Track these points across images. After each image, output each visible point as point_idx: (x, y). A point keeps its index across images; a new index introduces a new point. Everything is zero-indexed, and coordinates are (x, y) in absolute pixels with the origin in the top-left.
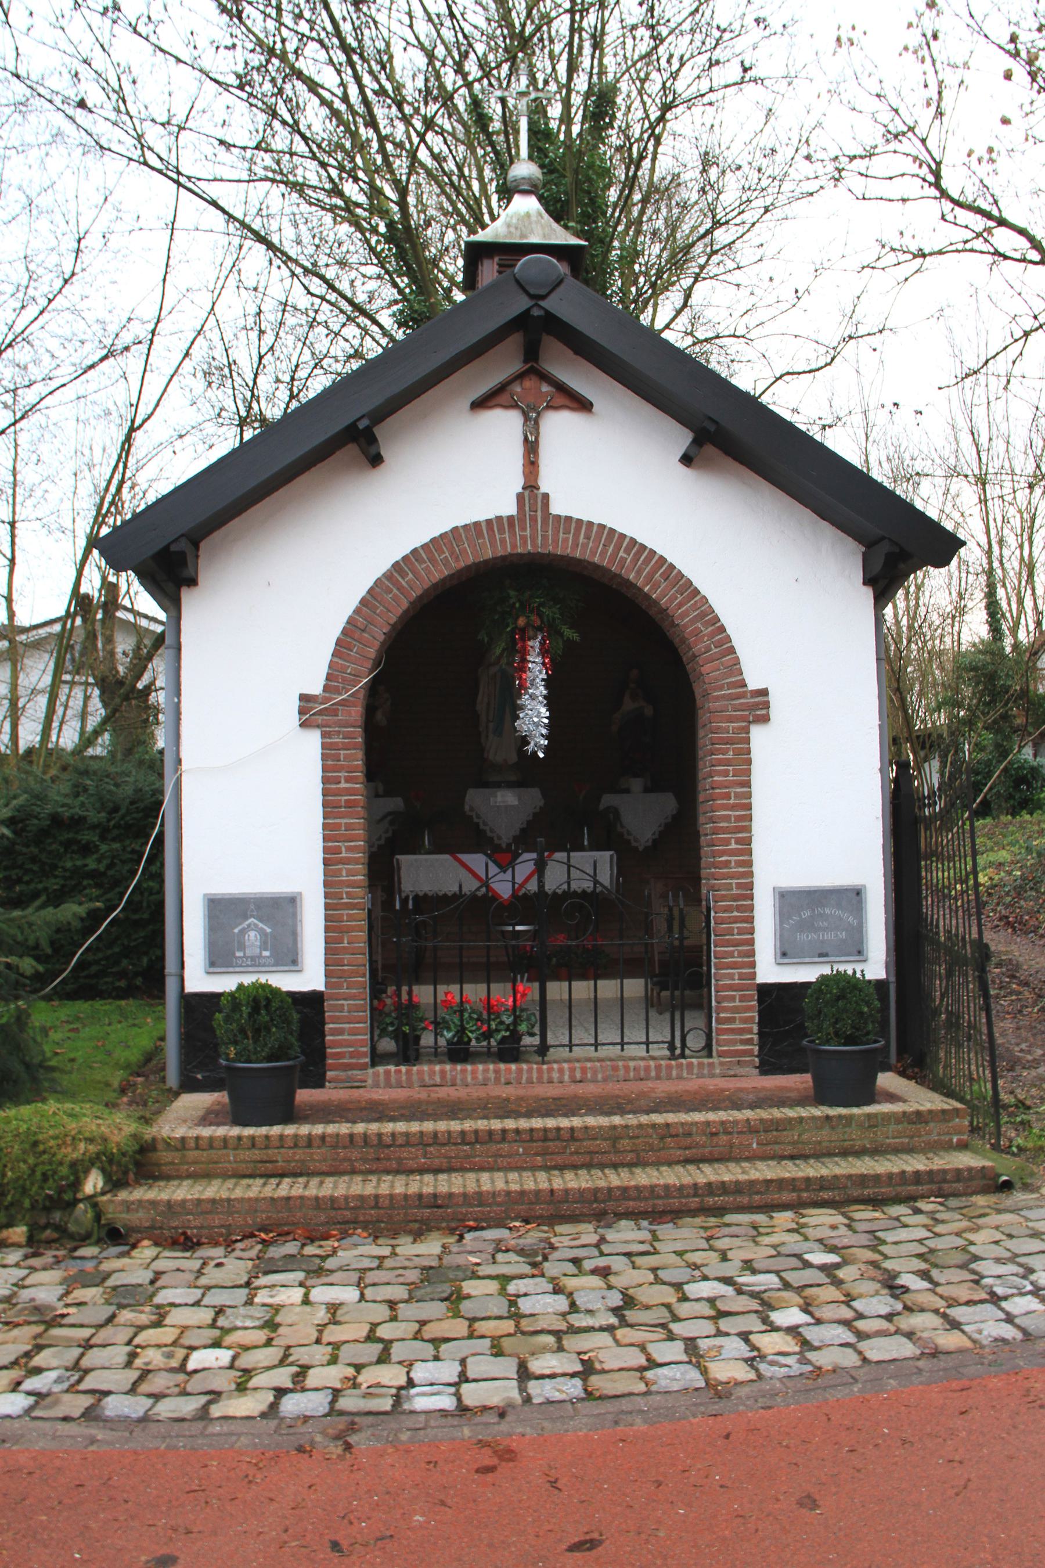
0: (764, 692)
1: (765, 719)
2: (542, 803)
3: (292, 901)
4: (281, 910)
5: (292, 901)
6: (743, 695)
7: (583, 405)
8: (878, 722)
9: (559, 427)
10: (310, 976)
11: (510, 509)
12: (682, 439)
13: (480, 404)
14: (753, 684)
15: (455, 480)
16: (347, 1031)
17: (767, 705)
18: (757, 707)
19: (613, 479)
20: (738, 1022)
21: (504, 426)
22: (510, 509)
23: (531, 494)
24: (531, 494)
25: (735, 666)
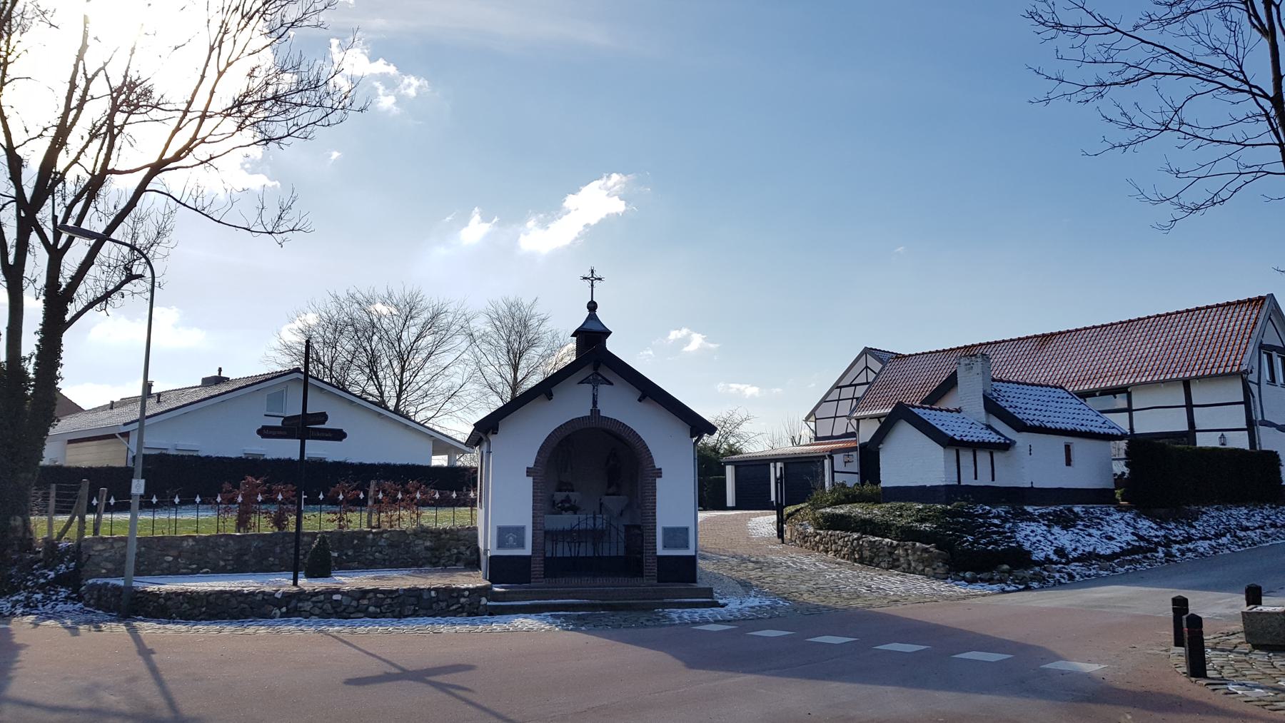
2: (101, 232)
3: (523, 528)
4: (519, 531)
5: (523, 528)
7: (611, 384)
8: (1282, 468)
9: (603, 389)
10: (527, 551)
11: (588, 414)
12: (639, 394)
13: (581, 382)
14: (531, 479)
15: (573, 405)
16: (537, 567)
18: (659, 473)
19: (618, 406)
20: (651, 568)
22: (588, 414)
23: (595, 411)
24: (595, 411)
25: (652, 462)
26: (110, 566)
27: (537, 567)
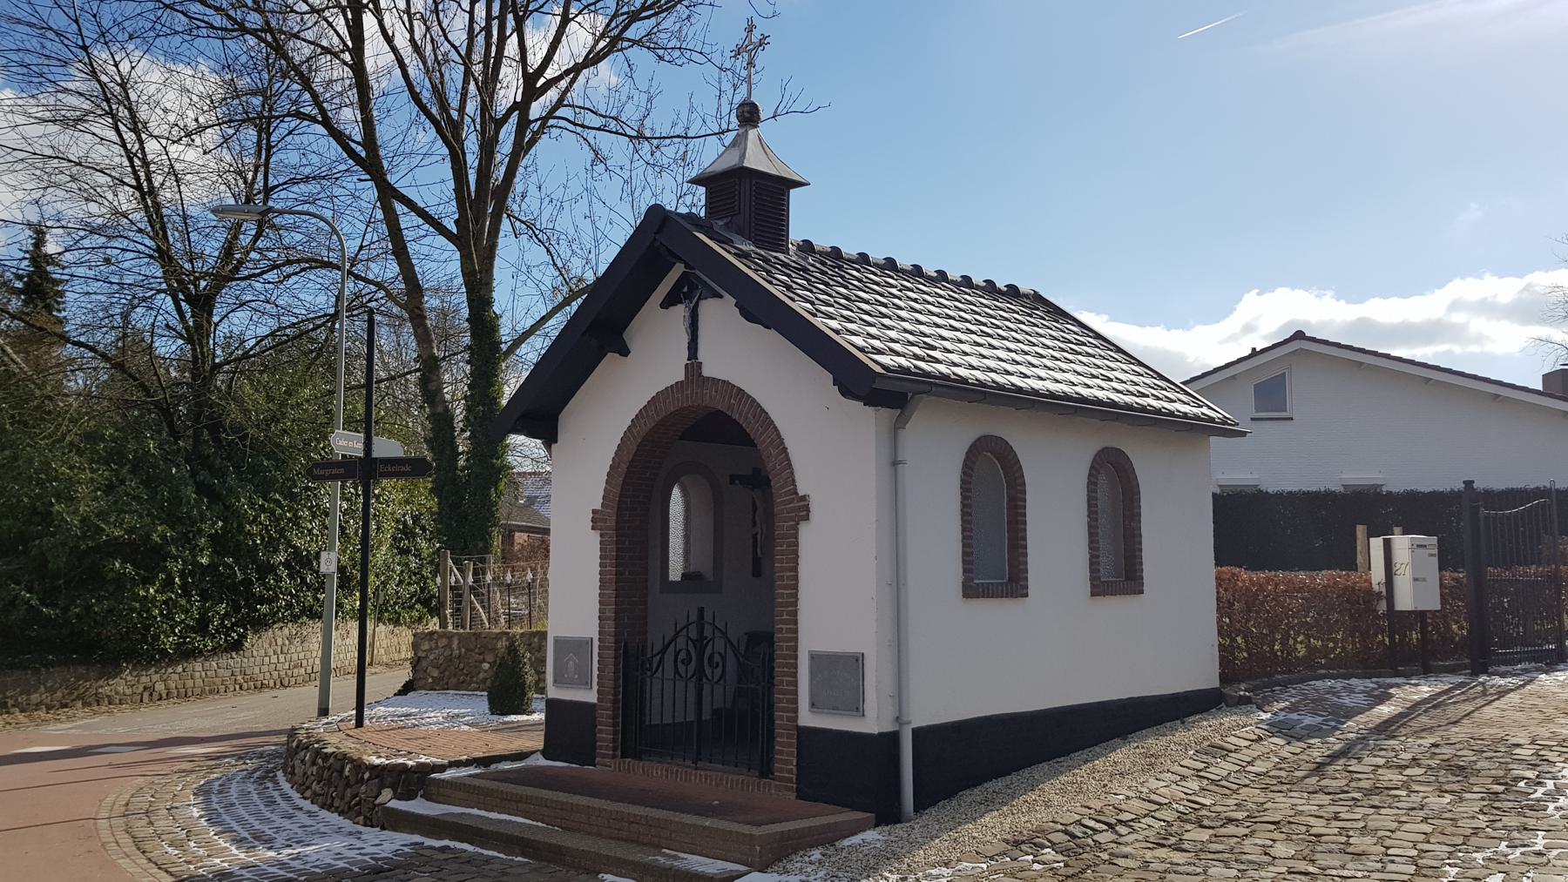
0: (804, 498)
1: (807, 518)
3: (857, 661)
6: (792, 501)
9: (708, 308)
10: (591, 696)
13: (668, 303)
16: (605, 733)
17: (807, 509)
21: (680, 311)
23: (693, 366)
24: (693, 366)
27: (605, 733)
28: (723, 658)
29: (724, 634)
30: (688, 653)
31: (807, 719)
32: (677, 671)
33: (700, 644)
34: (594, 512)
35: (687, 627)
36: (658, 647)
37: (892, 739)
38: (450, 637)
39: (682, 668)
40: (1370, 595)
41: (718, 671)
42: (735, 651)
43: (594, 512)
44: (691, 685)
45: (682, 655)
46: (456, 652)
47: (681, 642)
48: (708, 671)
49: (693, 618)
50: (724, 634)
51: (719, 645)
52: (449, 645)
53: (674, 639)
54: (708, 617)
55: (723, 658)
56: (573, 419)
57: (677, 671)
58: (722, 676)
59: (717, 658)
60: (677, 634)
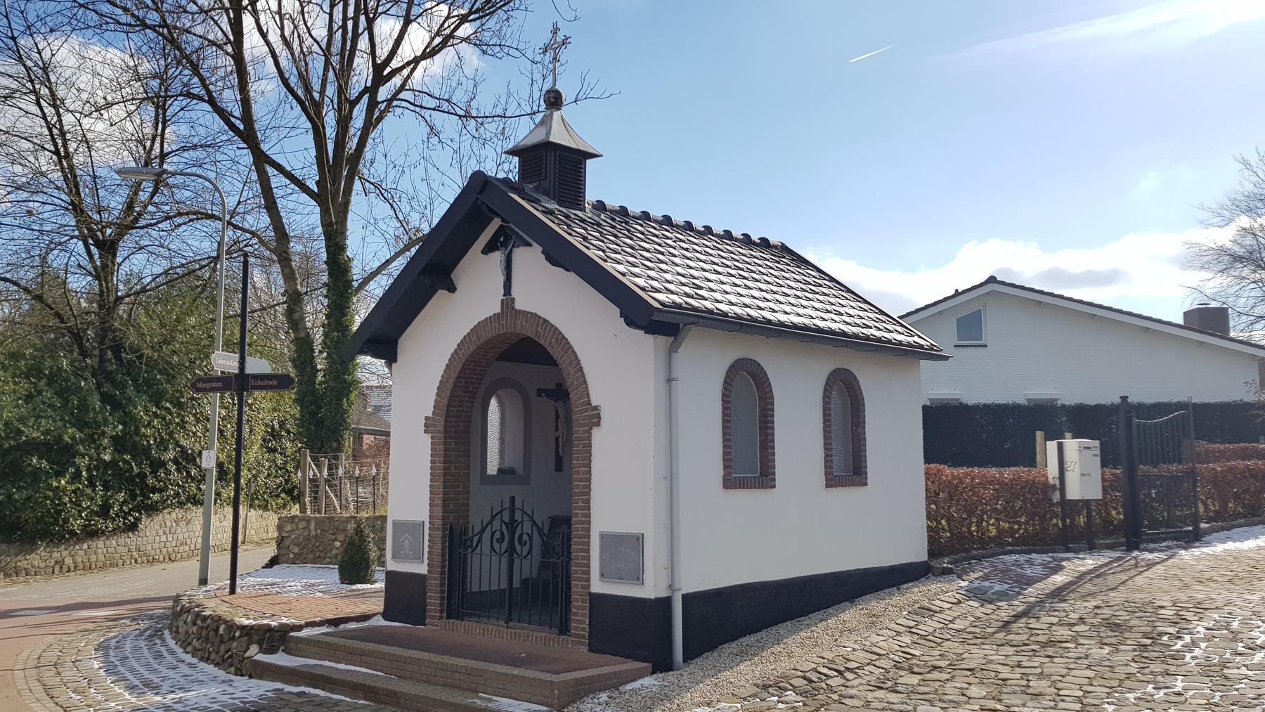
0: (596, 408)
1: (598, 424)
6: (586, 410)
10: (422, 569)
16: (434, 599)
21: (497, 257)
23: (508, 301)
26: (296, 550)
27: (434, 599)
28: (530, 537)
29: (531, 518)
30: (502, 533)
31: (598, 586)
32: (492, 548)
33: (512, 525)
34: (427, 418)
35: (501, 512)
36: (478, 529)
37: (666, 603)
38: (308, 520)
39: (496, 545)
40: (1046, 488)
41: (526, 548)
42: (540, 531)
43: (427, 418)
44: (504, 560)
45: (497, 535)
46: (313, 533)
47: (496, 524)
48: (518, 547)
49: (507, 505)
50: (531, 518)
51: (527, 526)
52: (307, 527)
53: (490, 522)
54: (518, 504)
55: (530, 537)
56: (409, 344)
57: (492, 548)
58: (530, 552)
59: (525, 538)
60: (493, 517)
